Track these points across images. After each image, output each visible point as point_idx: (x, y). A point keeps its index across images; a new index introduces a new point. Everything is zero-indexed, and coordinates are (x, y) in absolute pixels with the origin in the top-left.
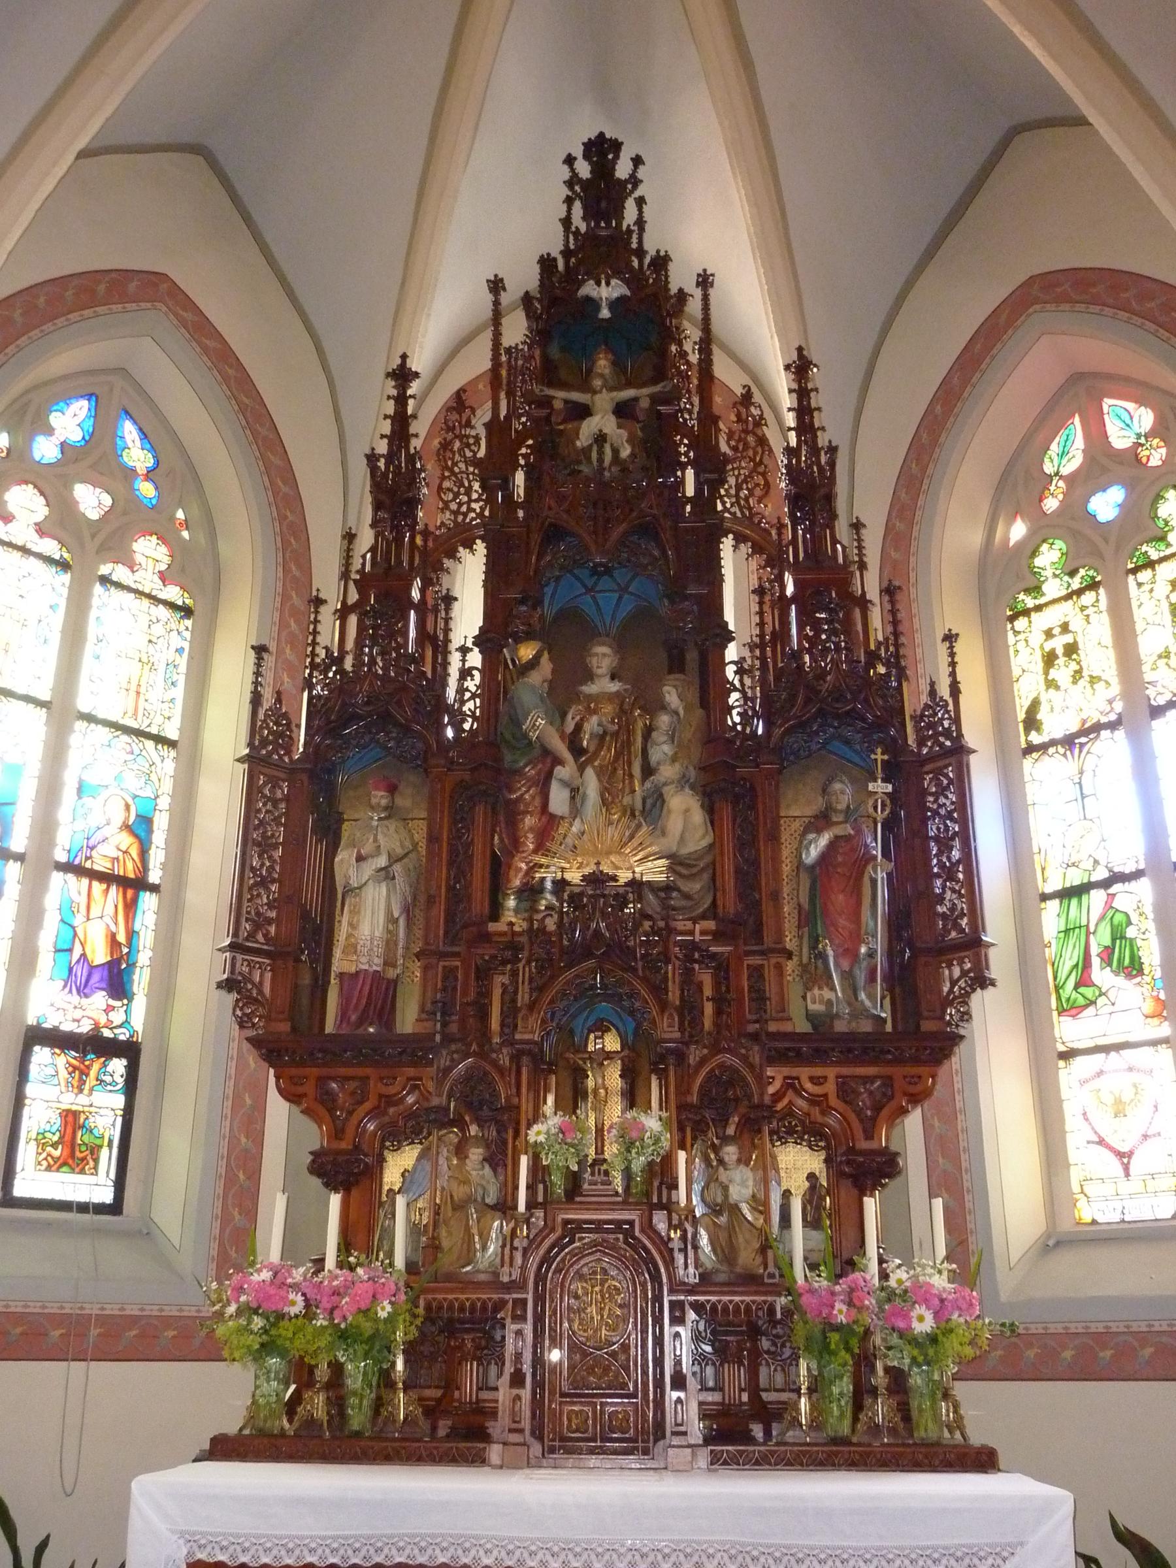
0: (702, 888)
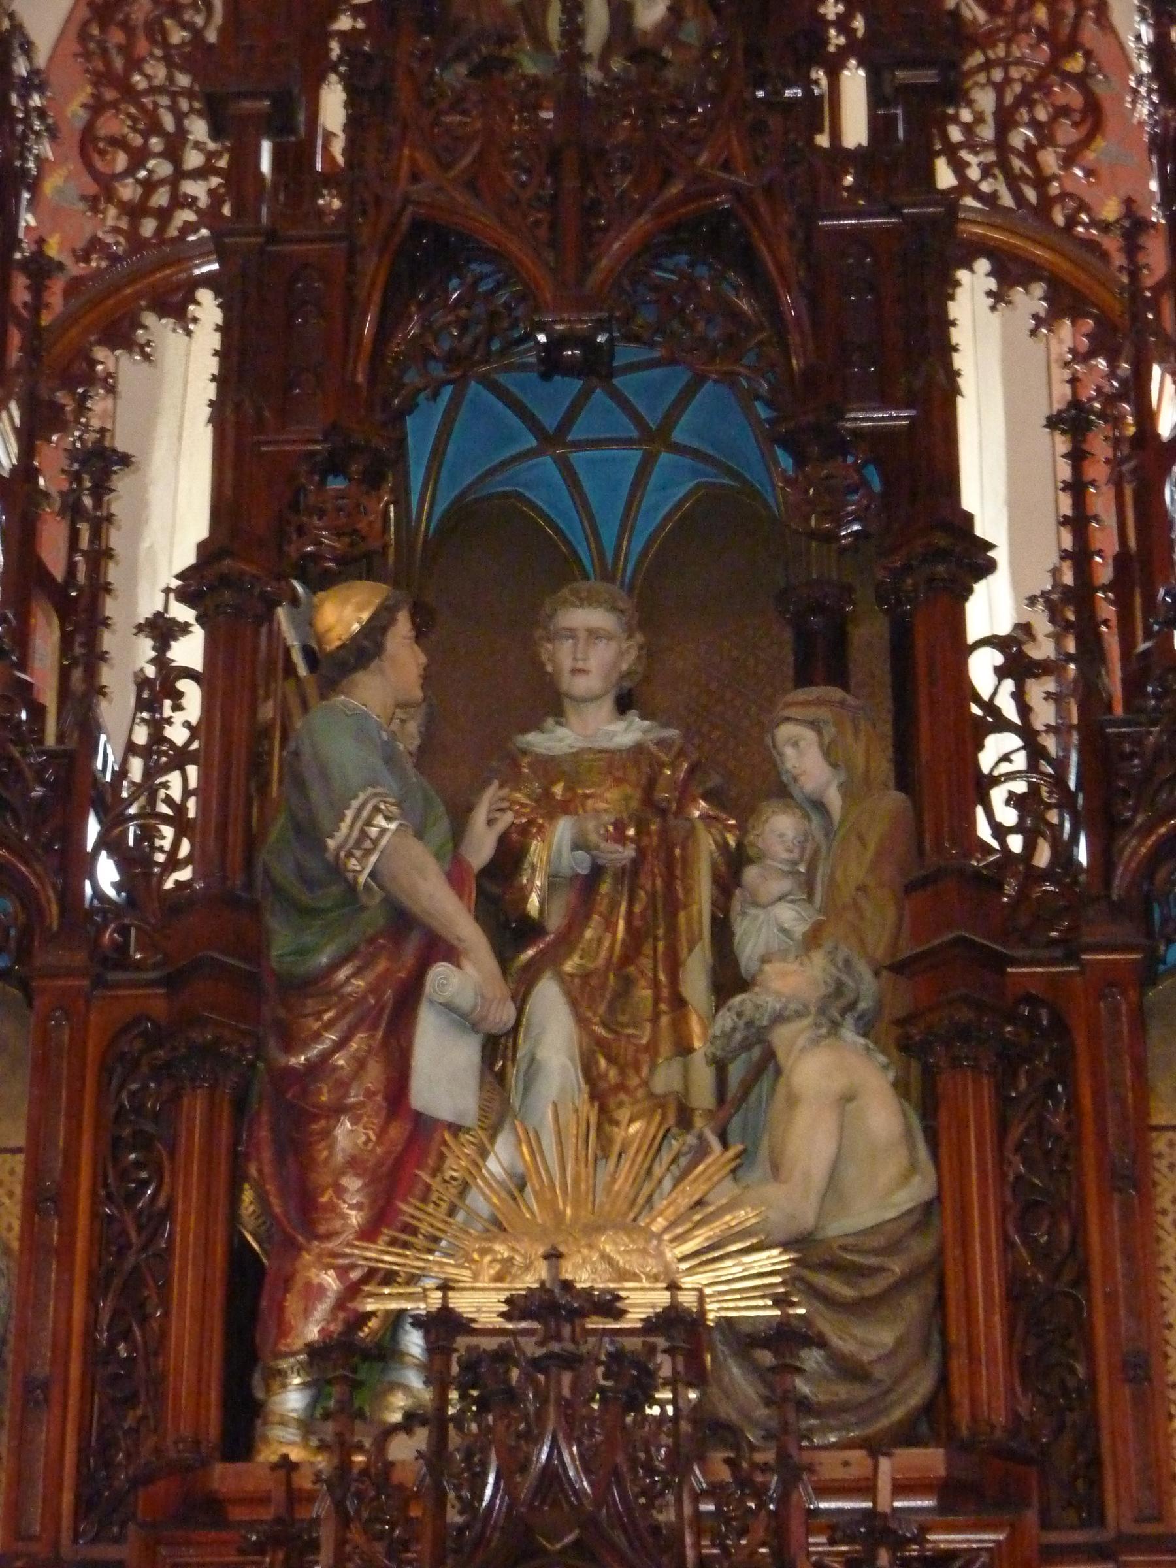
0: (900, 1342)
